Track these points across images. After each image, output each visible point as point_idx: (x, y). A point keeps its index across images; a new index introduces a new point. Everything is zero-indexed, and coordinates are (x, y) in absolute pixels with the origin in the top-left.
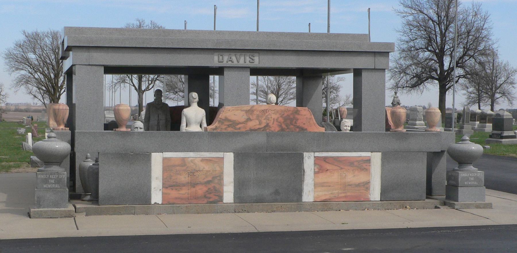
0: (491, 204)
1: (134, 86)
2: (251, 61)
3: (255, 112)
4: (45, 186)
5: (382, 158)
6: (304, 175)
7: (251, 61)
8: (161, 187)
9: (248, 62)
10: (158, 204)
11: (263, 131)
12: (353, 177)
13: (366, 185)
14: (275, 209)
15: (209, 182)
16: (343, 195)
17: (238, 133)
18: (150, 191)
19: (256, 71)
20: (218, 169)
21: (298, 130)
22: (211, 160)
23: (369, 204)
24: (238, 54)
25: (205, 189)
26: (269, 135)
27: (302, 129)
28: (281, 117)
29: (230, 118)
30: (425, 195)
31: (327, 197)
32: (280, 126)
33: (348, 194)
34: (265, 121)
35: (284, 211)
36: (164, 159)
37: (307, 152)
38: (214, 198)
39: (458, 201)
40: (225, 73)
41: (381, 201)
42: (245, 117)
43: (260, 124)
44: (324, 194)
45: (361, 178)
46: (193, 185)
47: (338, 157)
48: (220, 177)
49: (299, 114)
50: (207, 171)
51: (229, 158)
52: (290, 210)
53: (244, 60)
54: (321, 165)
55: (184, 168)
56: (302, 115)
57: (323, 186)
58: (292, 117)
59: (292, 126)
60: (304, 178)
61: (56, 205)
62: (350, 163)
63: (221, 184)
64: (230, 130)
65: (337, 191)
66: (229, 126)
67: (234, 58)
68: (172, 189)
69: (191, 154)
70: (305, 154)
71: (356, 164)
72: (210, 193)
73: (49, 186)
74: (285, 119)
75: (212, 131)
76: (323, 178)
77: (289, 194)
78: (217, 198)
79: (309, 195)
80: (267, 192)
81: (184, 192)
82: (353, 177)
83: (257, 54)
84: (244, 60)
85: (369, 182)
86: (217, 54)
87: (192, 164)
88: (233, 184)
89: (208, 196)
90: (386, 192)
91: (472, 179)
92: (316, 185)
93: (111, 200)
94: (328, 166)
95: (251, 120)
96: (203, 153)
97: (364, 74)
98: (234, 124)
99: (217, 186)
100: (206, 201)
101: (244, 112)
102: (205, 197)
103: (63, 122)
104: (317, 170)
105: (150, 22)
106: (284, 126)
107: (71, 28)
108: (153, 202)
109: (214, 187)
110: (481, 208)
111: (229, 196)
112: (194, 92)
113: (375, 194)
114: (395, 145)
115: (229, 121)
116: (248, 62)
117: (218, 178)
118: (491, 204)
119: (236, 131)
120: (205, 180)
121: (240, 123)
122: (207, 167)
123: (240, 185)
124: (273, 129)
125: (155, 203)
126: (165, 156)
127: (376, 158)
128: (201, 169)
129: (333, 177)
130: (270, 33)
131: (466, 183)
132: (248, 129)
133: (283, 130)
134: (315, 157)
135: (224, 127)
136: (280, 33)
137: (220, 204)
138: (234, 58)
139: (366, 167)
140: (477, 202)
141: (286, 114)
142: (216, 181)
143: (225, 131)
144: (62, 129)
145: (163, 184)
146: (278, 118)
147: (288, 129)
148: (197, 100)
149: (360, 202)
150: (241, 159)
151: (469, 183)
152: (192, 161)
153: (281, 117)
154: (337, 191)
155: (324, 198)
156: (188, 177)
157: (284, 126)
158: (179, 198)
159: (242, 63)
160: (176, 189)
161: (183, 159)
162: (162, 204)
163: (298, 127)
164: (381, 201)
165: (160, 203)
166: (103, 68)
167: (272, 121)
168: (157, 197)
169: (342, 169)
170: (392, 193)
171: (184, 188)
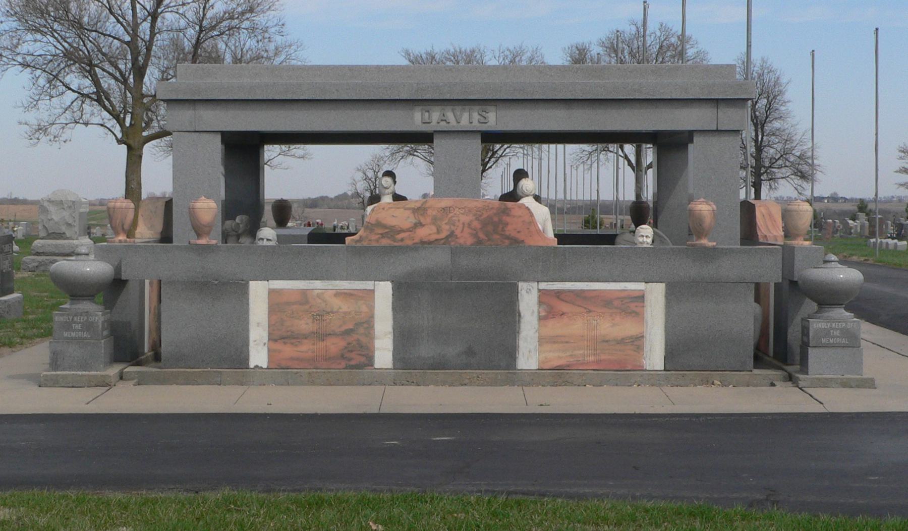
0: (872, 380)
1: (626, 157)
2: (483, 120)
3: (430, 212)
4: (66, 334)
6: (519, 321)
7: (483, 120)
8: (266, 340)
9: (475, 123)
10: (261, 368)
11: (444, 244)
12: (611, 327)
13: (637, 342)
14: (467, 381)
15: (348, 332)
16: (592, 358)
17: (400, 249)
18: (248, 345)
20: (364, 309)
21: (507, 242)
22: (351, 295)
24: (458, 108)
27: (515, 242)
28: (477, 219)
29: (384, 222)
30: (751, 362)
32: (475, 235)
33: (603, 357)
34: (447, 227)
35: (482, 385)
36: (272, 292)
37: (525, 281)
38: (357, 359)
39: (807, 374)
40: (436, 141)
42: (412, 220)
43: (438, 232)
44: (556, 356)
45: (627, 328)
46: (322, 336)
47: (583, 291)
48: (368, 323)
49: (508, 215)
50: (345, 313)
51: (384, 291)
52: (494, 383)
53: (469, 119)
54: (551, 305)
55: (307, 307)
56: (514, 216)
58: (496, 219)
59: (496, 237)
60: (519, 328)
61: (84, 366)
62: (606, 302)
64: (385, 242)
65: (581, 352)
66: (383, 236)
67: (450, 116)
68: (285, 343)
69: (318, 284)
70: (521, 285)
71: (616, 303)
72: (352, 351)
73: (73, 335)
74: (485, 224)
75: (354, 244)
76: (555, 327)
77: (497, 356)
78: (363, 359)
79: (528, 358)
80: (452, 351)
81: (306, 348)
82: (611, 327)
83: (492, 108)
84: (469, 119)
85: (643, 337)
87: (320, 301)
88: (391, 337)
89: (348, 355)
90: (675, 355)
91: (837, 333)
92: (542, 341)
93: (180, 360)
94: (564, 307)
95: (422, 225)
96: (334, 282)
98: (391, 232)
99: (364, 340)
100: (343, 364)
102: (342, 356)
103: (123, 228)
104: (543, 314)
105: (658, 26)
106: (482, 236)
108: (252, 365)
109: (358, 340)
110: (851, 387)
111: (384, 355)
114: (689, 269)
115: (385, 226)
116: (475, 123)
117: (365, 325)
118: (872, 380)
119: (396, 244)
120: (344, 328)
121: (402, 231)
122: (344, 306)
123: (404, 337)
124: (461, 241)
125: (257, 367)
126: (272, 287)
127: (656, 294)
128: (335, 310)
129: (575, 326)
131: (823, 340)
132: (417, 240)
133: (479, 242)
134: (539, 290)
135: (374, 237)
137: (367, 370)
138: (450, 116)
140: (846, 376)
141: (485, 216)
142: (361, 330)
144: (120, 241)
145: (270, 334)
146: (471, 221)
147: (489, 240)
149: (626, 371)
150: (404, 292)
151: (831, 341)
152: (318, 296)
154: (581, 352)
156: (313, 322)
157: (482, 236)
158: (297, 359)
160: (292, 344)
161: (304, 292)
162: (268, 368)
163: (508, 238)
164: (665, 370)
165: (265, 366)
166: (218, 138)
167: (461, 226)
168: (258, 357)
169: (590, 311)
170: (683, 356)
171: (306, 341)
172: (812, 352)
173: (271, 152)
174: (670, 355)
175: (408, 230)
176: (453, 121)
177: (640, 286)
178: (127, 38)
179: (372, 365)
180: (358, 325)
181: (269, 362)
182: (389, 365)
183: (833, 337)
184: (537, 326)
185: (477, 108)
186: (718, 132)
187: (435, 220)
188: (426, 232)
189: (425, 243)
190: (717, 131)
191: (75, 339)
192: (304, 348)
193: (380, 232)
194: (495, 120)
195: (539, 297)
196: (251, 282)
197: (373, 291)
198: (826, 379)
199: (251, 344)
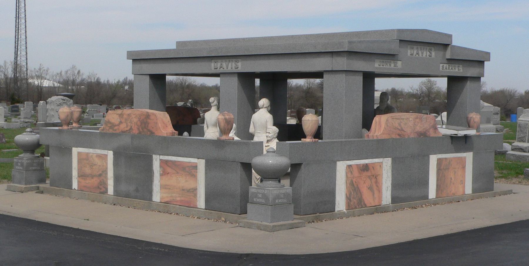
12: (183, 182)
13: (194, 191)
14: (135, 205)
15: (100, 175)
16: (178, 199)
26: (133, 137)
27: (152, 133)
32: (138, 129)
33: (182, 199)
37: (155, 154)
42: (119, 120)
43: (127, 127)
46: (92, 176)
47: (175, 161)
48: (105, 171)
49: (149, 119)
57: (165, 188)
59: (145, 130)
64: (111, 131)
66: (110, 127)
67: (224, 65)
69: (91, 151)
78: (104, 189)
79: (157, 197)
86: (220, 61)
88: (113, 179)
91: (260, 196)
94: (169, 170)
96: (97, 150)
98: (113, 125)
111: (111, 190)
112: (269, 100)
113: (201, 203)
115: (110, 123)
119: (114, 132)
120: (98, 173)
121: (116, 126)
124: (134, 131)
127: (201, 164)
130: (309, 35)
132: (120, 131)
133: (140, 133)
134: (160, 160)
138: (224, 65)
143: (108, 132)
151: (280, 201)
152: (92, 156)
159: (229, 70)
163: (149, 131)
166: (447, 78)
168: (75, 185)
169: (177, 173)
172: (249, 206)
173: (377, 80)
174: (207, 201)
176: (225, 69)
182: (112, 194)
188: (123, 127)
192: (87, 182)
197: (107, 155)
198: (251, 223)
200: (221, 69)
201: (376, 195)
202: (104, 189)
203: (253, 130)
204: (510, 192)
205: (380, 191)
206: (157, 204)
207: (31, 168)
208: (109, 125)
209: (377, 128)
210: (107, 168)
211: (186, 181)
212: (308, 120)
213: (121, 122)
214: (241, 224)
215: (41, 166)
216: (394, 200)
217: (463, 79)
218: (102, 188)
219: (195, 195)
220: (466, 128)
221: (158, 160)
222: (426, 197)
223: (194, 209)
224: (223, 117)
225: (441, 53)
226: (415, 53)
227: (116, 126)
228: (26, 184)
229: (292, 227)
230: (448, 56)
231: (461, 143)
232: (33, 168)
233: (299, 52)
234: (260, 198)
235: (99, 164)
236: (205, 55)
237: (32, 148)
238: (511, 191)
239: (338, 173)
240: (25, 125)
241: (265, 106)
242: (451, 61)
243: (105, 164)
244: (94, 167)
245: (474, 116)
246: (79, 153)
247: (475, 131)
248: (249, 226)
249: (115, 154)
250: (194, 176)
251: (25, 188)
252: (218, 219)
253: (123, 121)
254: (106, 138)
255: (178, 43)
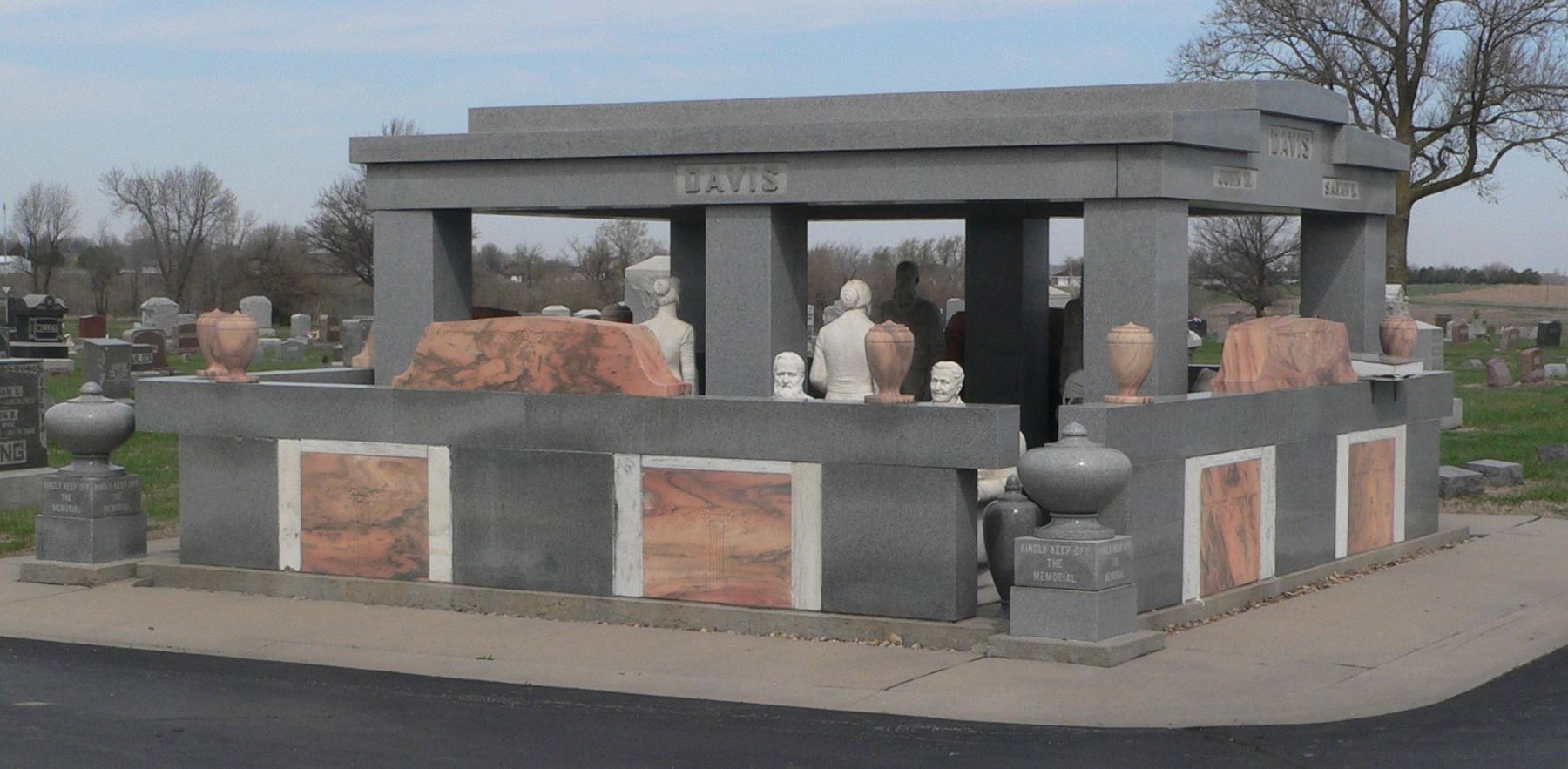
3: (497, 338)
4: (55, 508)
5: (823, 481)
8: (298, 529)
9: (759, 190)
12: (741, 534)
13: (780, 561)
14: (544, 610)
15: (396, 523)
16: (716, 585)
19: (1198, 209)
20: (416, 488)
21: (598, 388)
22: (399, 465)
23: (785, 618)
24: (736, 167)
25: (389, 540)
26: (533, 402)
27: (611, 389)
28: (558, 351)
31: (675, 588)
32: (555, 377)
33: (733, 583)
36: (305, 457)
37: (623, 452)
41: (822, 611)
42: (474, 351)
43: (508, 370)
44: (670, 578)
46: (364, 527)
48: (418, 510)
49: (599, 345)
51: (439, 459)
52: (580, 616)
53: (750, 185)
57: (665, 555)
58: (583, 352)
59: (584, 379)
63: (424, 531)
64: (441, 385)
66: (438, 375)
67: (724, 180)
69: (358, 447)
70: (619, 459)
71: (751, 494)
76: (667, 531)
77: (580, 570)
78: (415, 566)
79: (629, 581)
80: (528, 560)
81: (349, 545)
84: (750, 185)
85: (789, 553)
88: (449, 532)
91: (1058, 563)
92: (650, 551)
94: (679, 499)
97: (715, 228)
98: (448, 369)
99: (416, 536)
101: (470, 338)
104: (648, 507)
106: (564, 377)
107: (483, 109)
108: (282, 567)
111: (441, 565)
113: (807, 591)
115: (439, 360)
116: (759, 190)
117: (417, 513)
119: (454, 388)
120: (390, 517)
121: (462, 368)
123: (466, 534)
124: (537, 385)
127: (807, 480)
129: (694, 530)
130: (957, 93)
131: (1036, 575)
132: (481, 383)
133: (561, 388)
134: (643, 469)
135: (428, 377)
136: (985, 92)
139: (779, 506)
141: (568, 345)
142: (412, 521)
143: (428, 388)
146: (550, 354)
147: (575, 385)
148: (673, 294)
149: (755, 605)
151: (1049, 577)
152: (360, 465)
153: (558, 351)
155: (666, 589)
157: (564, 377)
161: (342, 459)
163: (599, 381)
164: (822, 611)
166: (431, 217)
167: (536, 364)
168: (290, 555)
169: (713, 507)
173: (813, 226)
174: (830, 583)
175: (469, 367)
176: (728, 191)
177: (783, 467)
178: (1392, 43)
179: (427, 576)
180: (408, 511)
181: (303, 561)
183: (1050, 571)
184: (640, 527)
185: (761, 167)
186: (1116, 201)
187: (504, 350)
188: (492, 371)
189: (492, 388)
190: (1116, 199)
191: (64, 514)
192: (343, 544)
193: (436, 368)
194: (788, 186)
195: (643, 480)
196: (281, 442)
197: (425, 461)
198: (1032, 644)
199: (282, 534)
200: (714, 192)
201: (1250, 553)
202: (415, 566)
203: (824, 374)
204: (1465, 536)
205: (1256, 541)
206: (634, 603)
207: (106, 509)
208: (435, 367)
209: (1243, 364)
210: (425, 500)
211: (747, 531)
212: (1132, 342)
213: (482, 358)
214: (993, 650)
215: (133, 499)
216: (1284, 564)
217: (1347, 221)
218: (406, 562)
219: (785, 572)
220: (1376, 357)
221: (636, 475)
222: (1330, 555)
223: (782, 612)
224: (889, 337)
225: (1315, 148)
226: (1281, 148)
227: (462, 368)
228: (95, 561)
229: (1144, 651)
230: (1340, 159)
231: (1386, 397)
232: (114, 508)
233: (1004, 143)
234: (1058, 570)
235: (392, 486)
236: (656, 150)
237: (100, 446)
238: (1467, 529)
239: (1187, 491)
240: (1537, 360)
241: (861, 303)
242: (1345, 170)
243: (416, 488)
244: (369, 499)
245: (1404, 325)
246: (305, 457)
247: (1421, 365)
248: (1027, 653)
249: (458, 456)
250: (780, 515)
251: (99, 571)
252: (881, 636)
253: (491, 352)
254: (421, 406)
255: (476, 115)
